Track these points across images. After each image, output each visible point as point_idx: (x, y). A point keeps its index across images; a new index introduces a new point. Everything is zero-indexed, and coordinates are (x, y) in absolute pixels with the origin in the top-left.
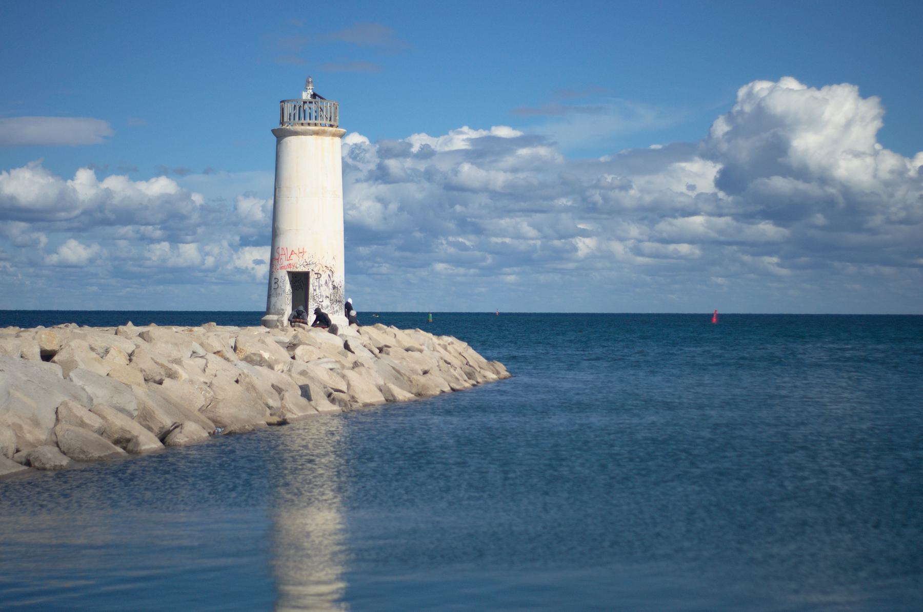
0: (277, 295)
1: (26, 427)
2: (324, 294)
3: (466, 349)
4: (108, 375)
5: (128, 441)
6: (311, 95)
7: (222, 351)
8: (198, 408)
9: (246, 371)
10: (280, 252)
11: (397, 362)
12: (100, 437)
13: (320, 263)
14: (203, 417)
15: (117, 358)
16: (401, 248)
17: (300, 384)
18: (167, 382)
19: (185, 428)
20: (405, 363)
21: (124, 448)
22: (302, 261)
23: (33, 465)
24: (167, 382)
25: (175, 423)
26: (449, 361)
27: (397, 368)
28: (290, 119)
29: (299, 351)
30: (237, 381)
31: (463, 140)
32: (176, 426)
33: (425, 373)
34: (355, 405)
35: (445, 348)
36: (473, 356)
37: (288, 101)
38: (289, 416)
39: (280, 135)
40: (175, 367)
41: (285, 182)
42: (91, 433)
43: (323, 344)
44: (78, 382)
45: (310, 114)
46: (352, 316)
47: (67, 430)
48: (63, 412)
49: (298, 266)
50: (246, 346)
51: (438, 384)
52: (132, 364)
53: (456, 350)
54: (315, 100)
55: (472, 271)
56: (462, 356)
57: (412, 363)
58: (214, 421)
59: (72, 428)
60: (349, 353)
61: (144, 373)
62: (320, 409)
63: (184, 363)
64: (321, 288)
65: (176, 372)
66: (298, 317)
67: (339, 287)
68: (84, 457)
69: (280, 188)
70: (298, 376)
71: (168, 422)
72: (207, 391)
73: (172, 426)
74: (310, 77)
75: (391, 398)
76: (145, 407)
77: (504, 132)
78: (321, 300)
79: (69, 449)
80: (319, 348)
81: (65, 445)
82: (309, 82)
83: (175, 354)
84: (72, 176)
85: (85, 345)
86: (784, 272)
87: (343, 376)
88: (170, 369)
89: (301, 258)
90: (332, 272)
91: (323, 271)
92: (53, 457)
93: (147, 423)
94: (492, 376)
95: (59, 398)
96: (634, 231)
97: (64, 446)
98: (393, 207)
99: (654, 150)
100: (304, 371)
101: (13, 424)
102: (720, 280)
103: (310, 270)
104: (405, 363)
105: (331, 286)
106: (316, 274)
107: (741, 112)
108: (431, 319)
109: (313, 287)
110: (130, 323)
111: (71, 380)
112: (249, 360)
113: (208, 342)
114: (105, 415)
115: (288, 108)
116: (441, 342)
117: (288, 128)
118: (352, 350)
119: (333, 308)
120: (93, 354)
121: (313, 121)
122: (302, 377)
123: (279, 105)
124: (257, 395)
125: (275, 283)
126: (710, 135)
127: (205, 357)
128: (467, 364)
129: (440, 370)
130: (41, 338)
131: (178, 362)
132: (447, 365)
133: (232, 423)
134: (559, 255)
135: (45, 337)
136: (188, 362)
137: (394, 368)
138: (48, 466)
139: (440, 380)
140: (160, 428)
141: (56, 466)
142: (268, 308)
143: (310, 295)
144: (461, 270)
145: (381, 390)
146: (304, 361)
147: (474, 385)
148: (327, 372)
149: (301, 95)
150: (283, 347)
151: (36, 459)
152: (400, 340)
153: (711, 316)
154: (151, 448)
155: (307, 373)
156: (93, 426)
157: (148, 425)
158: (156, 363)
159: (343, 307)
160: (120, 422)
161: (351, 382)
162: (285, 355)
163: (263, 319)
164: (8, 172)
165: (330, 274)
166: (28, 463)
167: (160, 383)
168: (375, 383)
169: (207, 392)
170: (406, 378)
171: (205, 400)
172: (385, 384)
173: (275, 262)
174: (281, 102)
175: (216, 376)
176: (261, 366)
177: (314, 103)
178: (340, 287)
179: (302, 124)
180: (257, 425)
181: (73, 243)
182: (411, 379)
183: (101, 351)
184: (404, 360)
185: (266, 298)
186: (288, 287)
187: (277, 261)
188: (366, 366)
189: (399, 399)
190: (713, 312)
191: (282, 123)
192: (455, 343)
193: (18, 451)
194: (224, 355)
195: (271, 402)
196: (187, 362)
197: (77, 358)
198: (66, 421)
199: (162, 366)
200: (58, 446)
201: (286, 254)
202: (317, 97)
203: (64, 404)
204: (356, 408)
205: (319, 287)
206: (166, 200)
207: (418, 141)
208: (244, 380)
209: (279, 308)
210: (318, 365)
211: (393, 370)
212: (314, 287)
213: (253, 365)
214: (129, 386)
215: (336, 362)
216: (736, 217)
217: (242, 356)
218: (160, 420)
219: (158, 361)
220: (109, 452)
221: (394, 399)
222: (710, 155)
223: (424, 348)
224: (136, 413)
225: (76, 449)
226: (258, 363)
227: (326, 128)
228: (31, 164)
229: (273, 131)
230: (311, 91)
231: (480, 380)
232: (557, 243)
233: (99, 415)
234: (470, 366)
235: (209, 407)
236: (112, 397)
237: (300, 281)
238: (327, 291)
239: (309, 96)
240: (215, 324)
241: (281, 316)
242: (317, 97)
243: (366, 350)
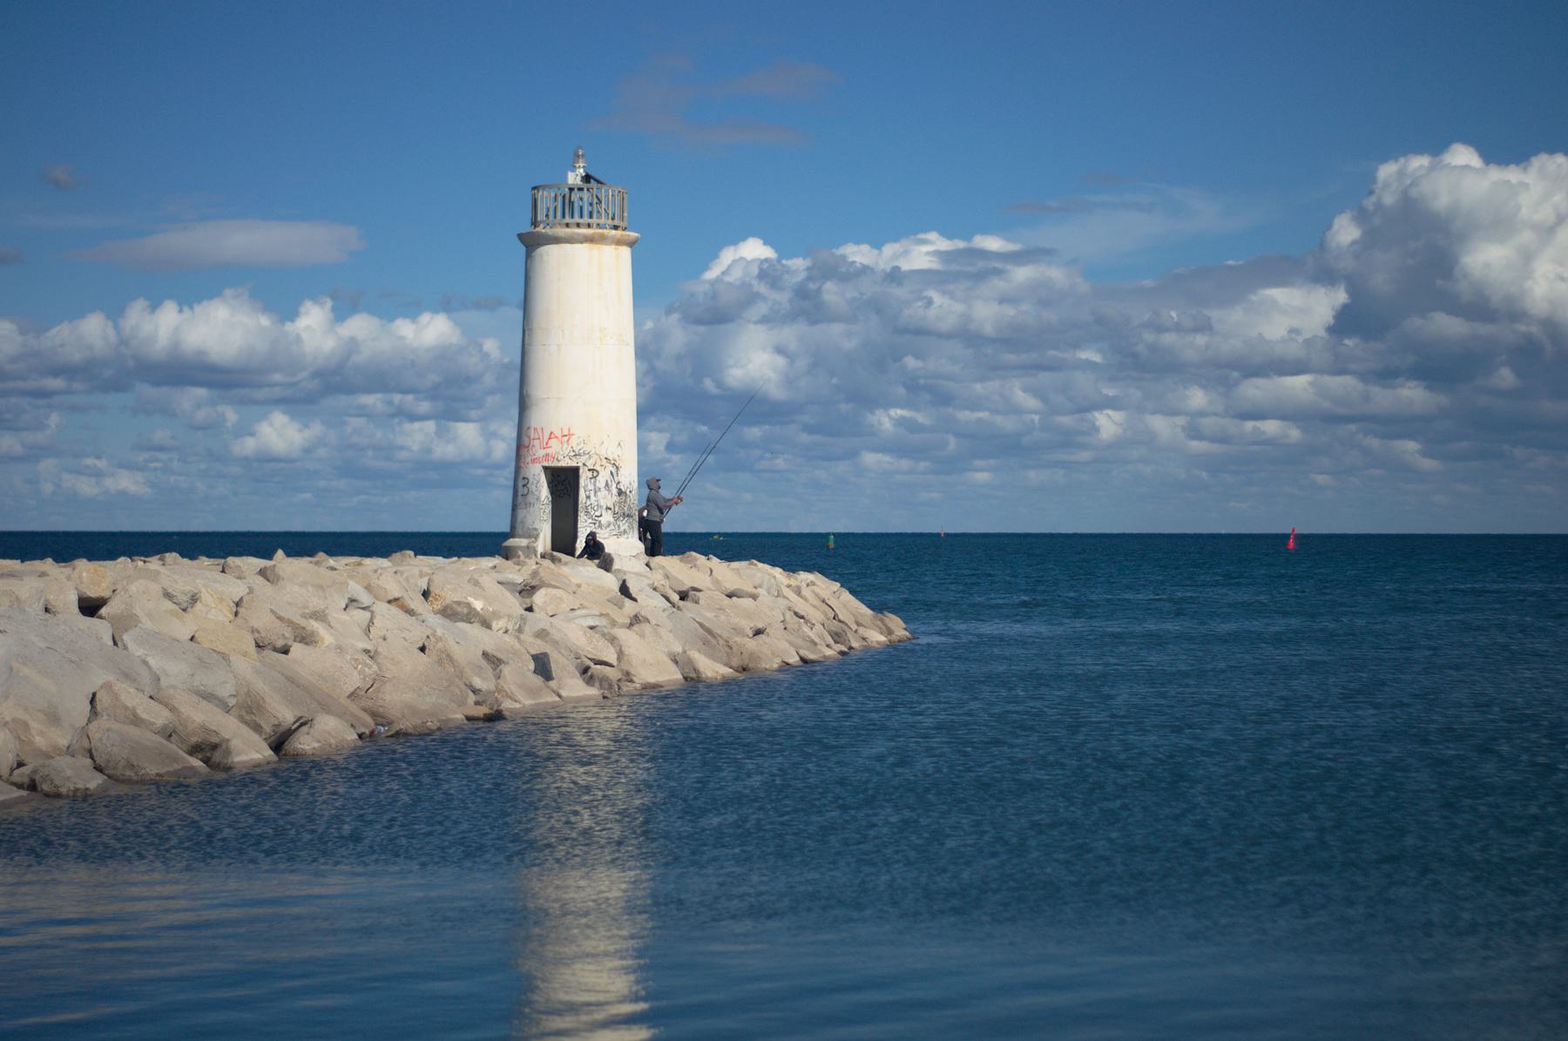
0: (526, 504)
1: (34, 725)
3: (837, 594)
4: (192, 639)
5: (215, 747)
6: (582, 177)
7: (402, 597)
8: (348, 693)
9: (439, 632)
11: (709, 615)
12: (165, 742)
13: (596, 454)
14: (353, 708)
15: (213, 610)
16: (809, 429)
17: (533, 652)
18: (297, 649)
19: (316, 727)
20: (723, 617)
21: (207, 761)
22: (566, 450)
23: (39, 789)
24: (297, 649)
25: (301, 718)
26: (802, 613)
27: (706, 624)
28: (547, 216)
29: (539, 598)
30: (423, 649)
31: (928, 253)
32: (303, 723)
33: (758, 632)
34: (627, 686)
35: (798, 592)
36: (848, 605)
37: (544, 187)
38: (507, 705)
39: (532, 243)
40: (315, 625)
41: (539, 321)
42: (149, 735)
43: (584, 587)
44: (137, 651)
45: (581, 208)
47: (108, 730)
48: (104, 700)
49: (560, 457)
50: (445, 589)
51: (779, 651)
52: (239, 620)
53: (817, 595)
54: (588, 185)
55: (923, 465)
56: (826, 604)
57: (740, 615)
58: (374, 715)
59: (116, 726)
60: (628, 602)
61: (256, 635)
62: (564, 694)
63: (330, 618)
64: (599, 493)
65: (313, 634)
66: (563, 542)
67: (628, 492)
68: (133, 774)
69: (530, 330)
70: (531, 640)
71: (287, 716)
72: (366, 665)
73: (295, 723)
74: (580, 147)
75: (694, 675)
76: (249, 690)
77: (993, 244)
78: (598, 513)
79: (109, 762)
80: (574, 593)
81: (103, 755)
82: (578, 156)
83: (316, 603)
84: (291, 314)
85: (155, 588)
86: (1429, 464)
87: (613, 640)
88: (304, 628)
89: (565, 445)
90: (617, 468)
91: (602, 466)
92: (78, 776)
93: (254, 718)
94: (877, 638)
95: (98, 678)
96: (1197, 398)
97: (101, 757)
98: (802, 363)
99: (1230, 267)
100: (544, 630)
101: (13, 720)
102: (1321, 479)
103: (580, 464)
104: (723, 617)
105: (615, 491)
106: (589, 470)
107: (1379, 206)
108: (831, 544)
110: (280, 553)
111: (126, 648)
112: (449, 613)
113: (380, 583)
114: (176, 705)
115: (546, 199)
116: (793, 582)
117: (544, 231)
118: (634, 595)
119: (619, 526)
120: (169, 605)
121: (586, 220)
122: (539, 641)
123: (529, 193)
124: (455, 671)
125: (524, 486)
126: (1322, 246)
127: (371, 609)
128: (834, 618)
129: (785, 629)
130: (80, 577)
131: (319, 616)
132: (798, 619)
133: (404, 716)
134: (1068, 440)
135: (89, 575)
136: (337, 615)
137: (701, 625)
138: (63, 790)
139: (784, 645)
140: (274, 725)
141: (77, 790)
142: (513, 527)
144: (905, 464)
145: (676, 662)
146: (547, 614)
147: (842, 653)
148: (585, 632)
149: (566, 178)
150: (512, 591)
151: (45, 778)
152: (720, 578)
153: (1285, 537)
154: (251, 760)
155: (548, 634)
156: (152, 724)
157: (255, 721)
158: (280, 618)
159: (636, 525)
160: (200, 716)
161: (626, 650)
162: (514, 604)
164: (191, 308)
165: (614, 470)
166: (32, 786)
167: (285, 651)
168: (666, 650)
169: (366, 666)
170: (721, 642)
171: (364, 679)
172: (684, 652)
173: (524, 451)
174: (534, 188)
175: (385, 639)
176: (470, 623)
177: (585, 189)
178: (630, 492)
179: (567, 225)
180: (449, 720)
181: (279, 418)
182: (731, 643)
183: (183, 599)
184: (721, 611)
185: (510, 508)
186: (544, 493)
188: (653, 622)
189: (707, 678)
190: (1290, 531)
191: (535, 223)
192: (818, 583)
193: (20, 764)
194: (406, 604)
195: (478, 683)
196: (337, 616)
197: (138, 611)
198: (108, 715)
199: (290, 623)
200: (92, 757)
202: (592, 181)
203: (108, 686)
204: (627, 691)
205: (595, 492)
206: (443, 354)
207: (859, 254)
208: (434, 646)
210: (569, 620)
211: (700, 630)
212: (587, 493)
213: (455, 622)
214: (224, 657)
215: (601, 615)
216: (1363, 376)
217: (438, 606)
218: (273, 712)
219: (282, 614)
220: (176, 767)
221: (698, 677)
222: (1325, 276)
223: (761, 591)
224: (232, 702)
225: (119, 761)
226: (465, 618)
227: (605, 231)
228: (228, 292)
229: (521, 237)
230: (582, 170)
231: (855, 644)
232: (1066, 420)
233: (166, 705)
234: (840, 621)
235: (371, 690)
236: (193, 675)
237: (564, 482)
238: (607, 499)
239: (579, 179)
240: (412, 553)
241: (533, 539)
242: (592, 181)
243: (657, 595)
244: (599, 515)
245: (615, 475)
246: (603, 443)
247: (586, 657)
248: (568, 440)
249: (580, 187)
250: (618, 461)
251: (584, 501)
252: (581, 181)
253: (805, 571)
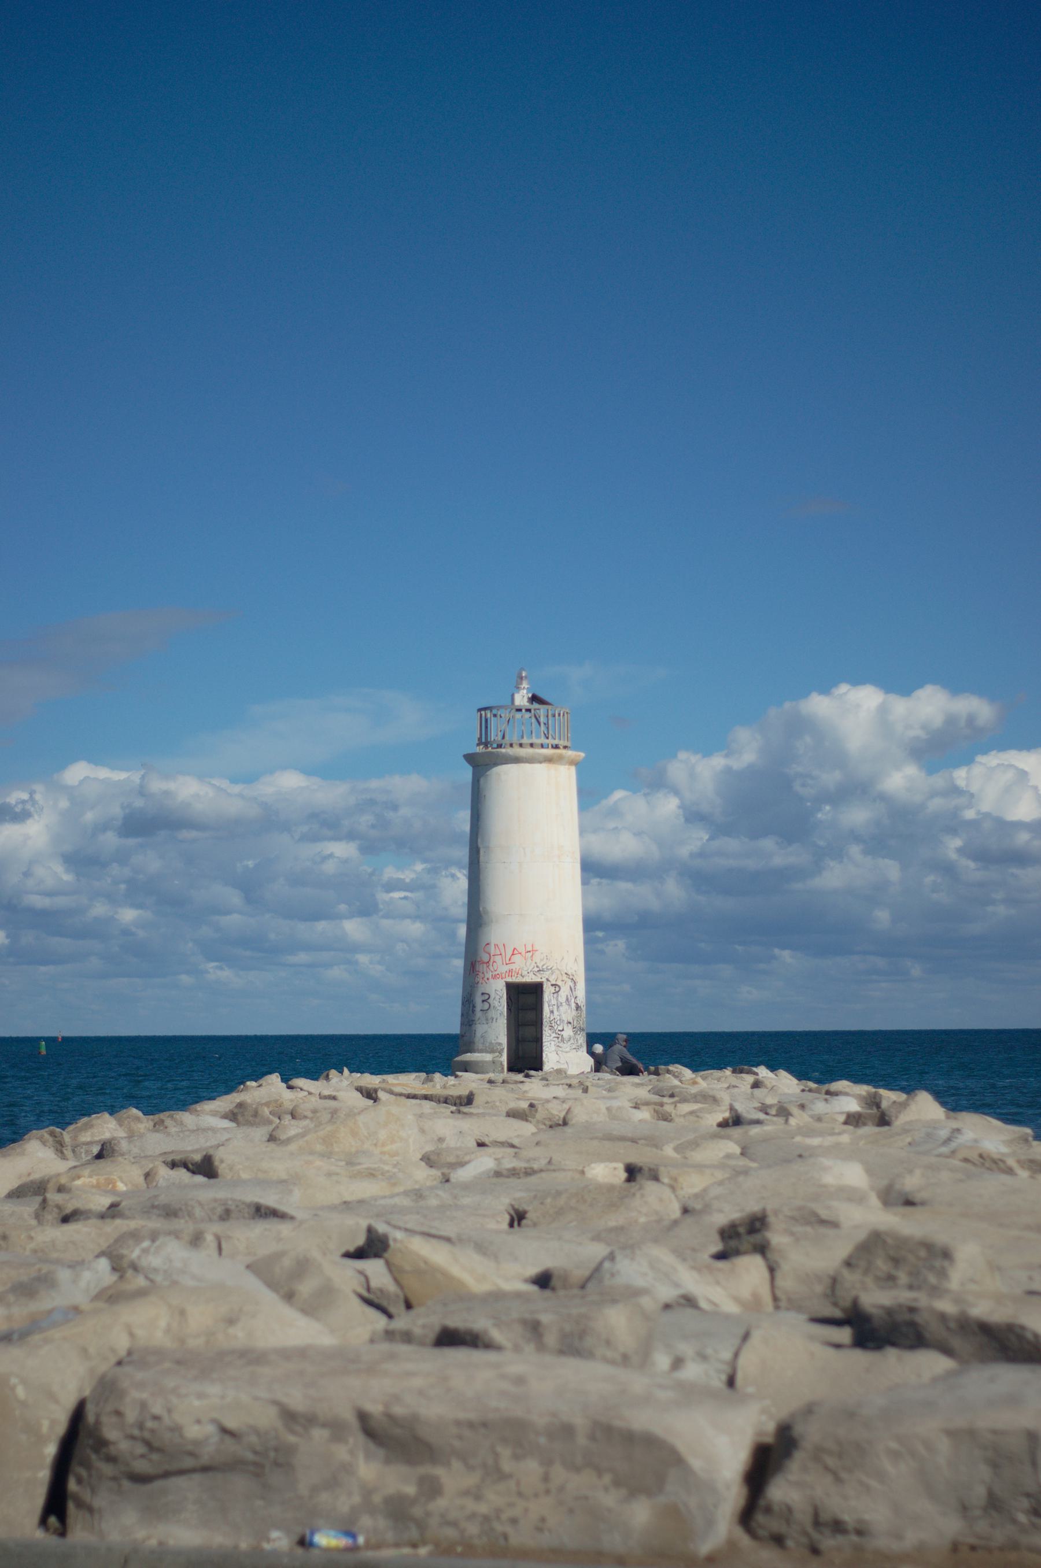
2: (565, 1018)
6: (529, 698)
10: (492, 950)
13: (558, 969)
23: (11, 1298)
46: (598, 1054)
64: (561, 1008)
74: (522, 669)
82: (521, 678)
89: (529, 961)
90: (575, 983)
91: (563, 981)
103: (544, 980)
105: (573, 1005)
106: (552, 985)
109: (549, 1006)
125: (483, 1001)
143: (544, 1020)
174: (480, 710)
187: (485, 965)
201: (503, 954)
205: (558, 1007)
209: (493, 1041)
238: (567, 1013)
239: (526, 700)
244: (561, 1029)
245: (573, 990)
246: (563, 958)
247: (337, 1174)
248: (532, 956)
249: (527, 708)
250: (575, 976)
251: (548, 1016)
252: (528, 702)
253: (297, 1078)
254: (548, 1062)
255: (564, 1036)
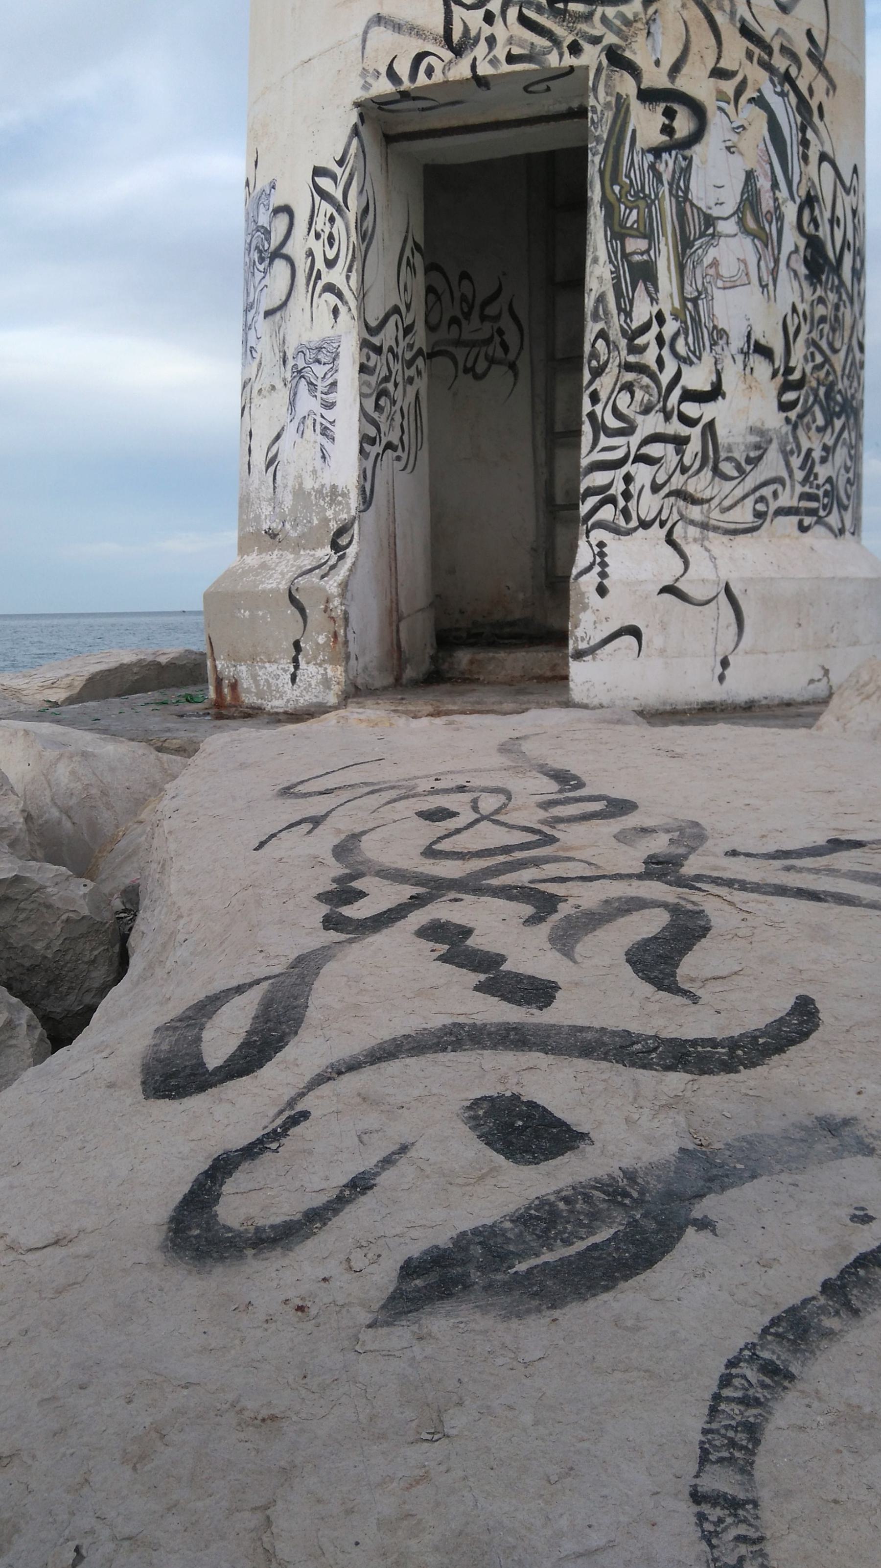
41: (295, 284)
91: (718, 73)
99: (555, 1128)
106: (648, 96)
163: (447, 947)
205: (684, 243)
245: (794, 150)
254: (602, 591)
255: (721, 432)
